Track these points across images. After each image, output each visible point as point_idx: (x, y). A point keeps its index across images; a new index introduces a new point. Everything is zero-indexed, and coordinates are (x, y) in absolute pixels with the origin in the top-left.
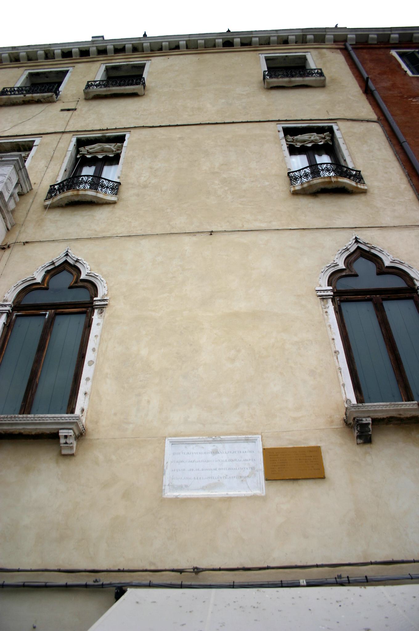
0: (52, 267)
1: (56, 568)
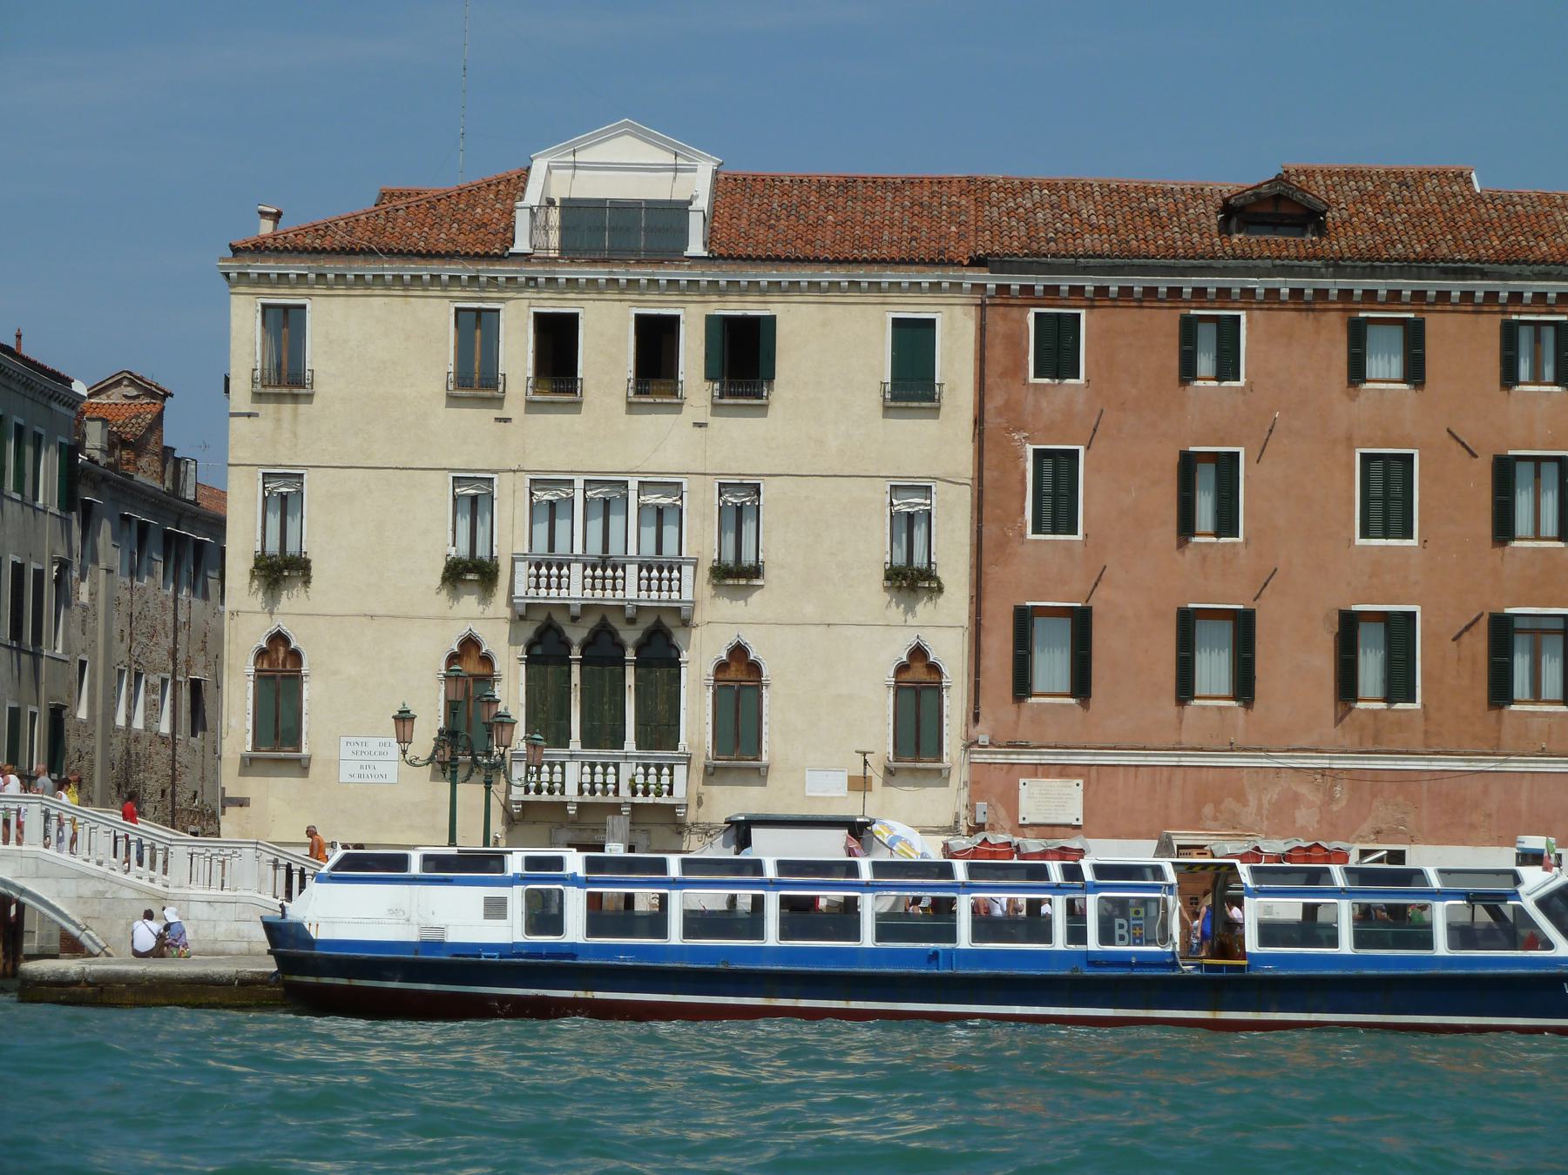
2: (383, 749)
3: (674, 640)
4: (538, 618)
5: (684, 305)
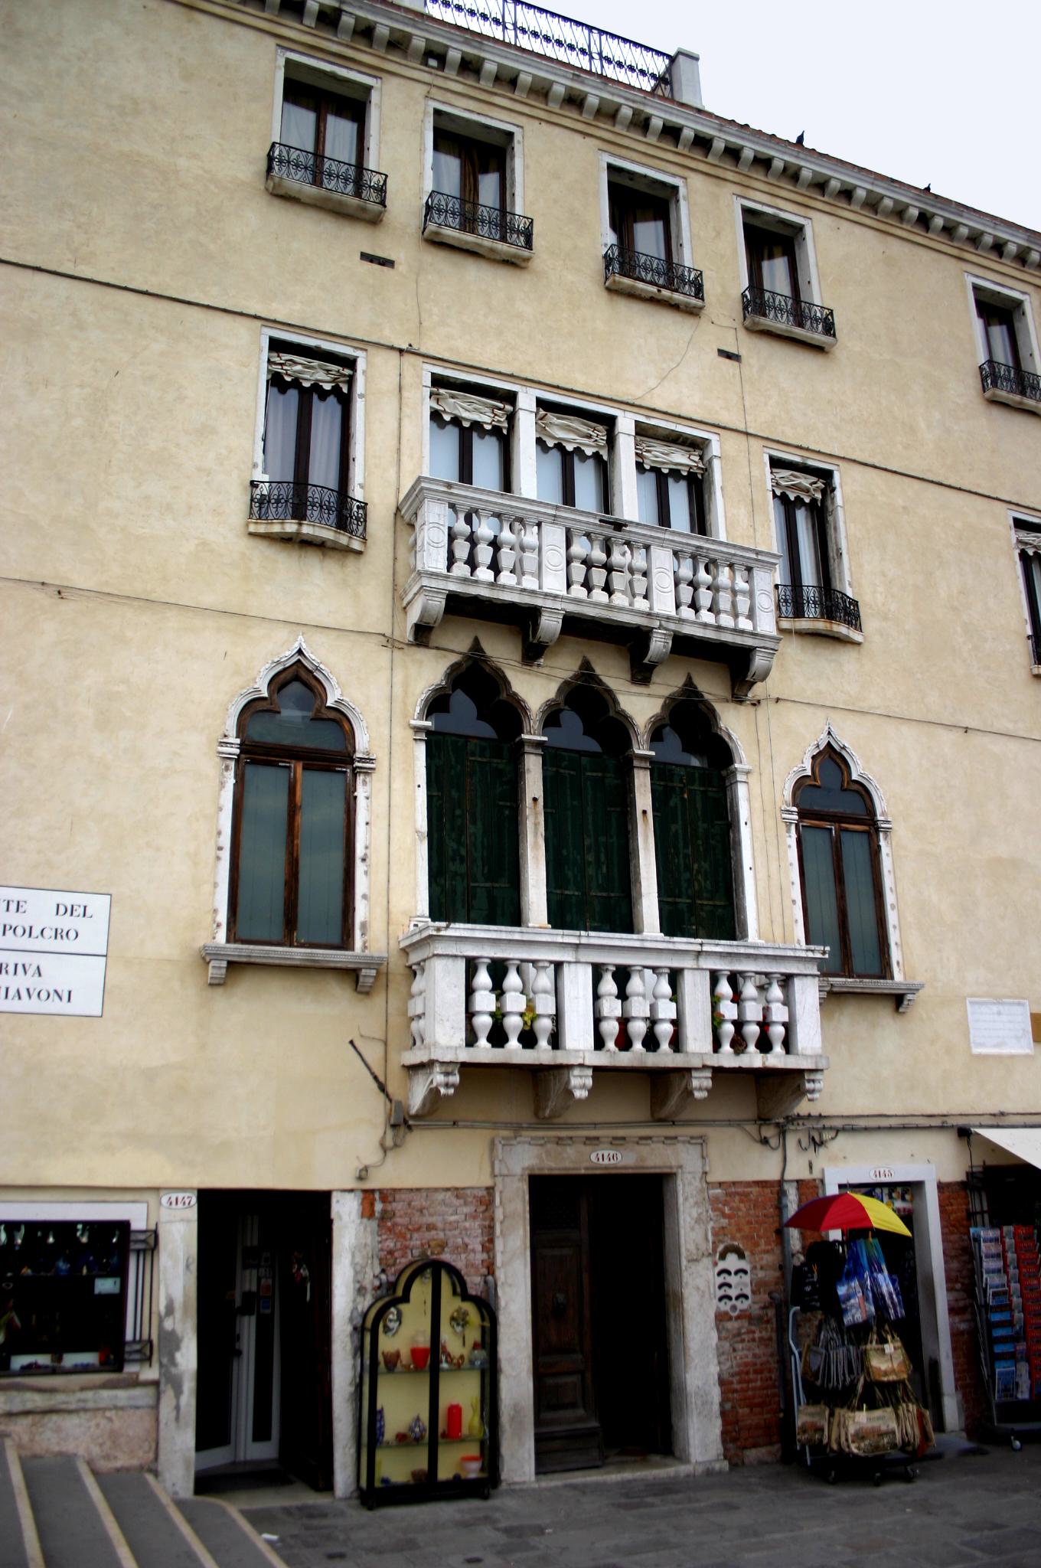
1: (919, 1113)
2: (65, 922)
3: (722, 725)
4: (456, 649)
5: (687, 173)
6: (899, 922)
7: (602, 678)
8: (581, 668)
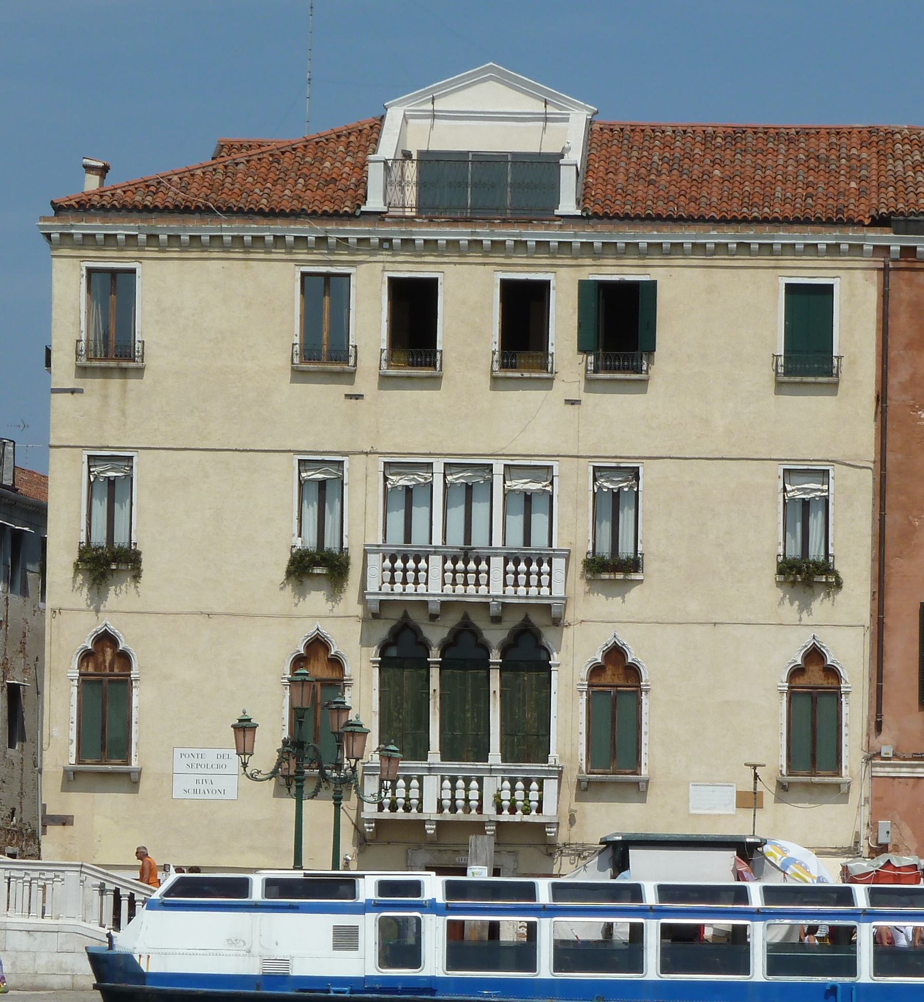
0: (607, 647)
2: (221, 762)
3: (544, 640)
5: (555, 269)
6: (649, 741)
7: (474, 622)
8: (462, 619)
